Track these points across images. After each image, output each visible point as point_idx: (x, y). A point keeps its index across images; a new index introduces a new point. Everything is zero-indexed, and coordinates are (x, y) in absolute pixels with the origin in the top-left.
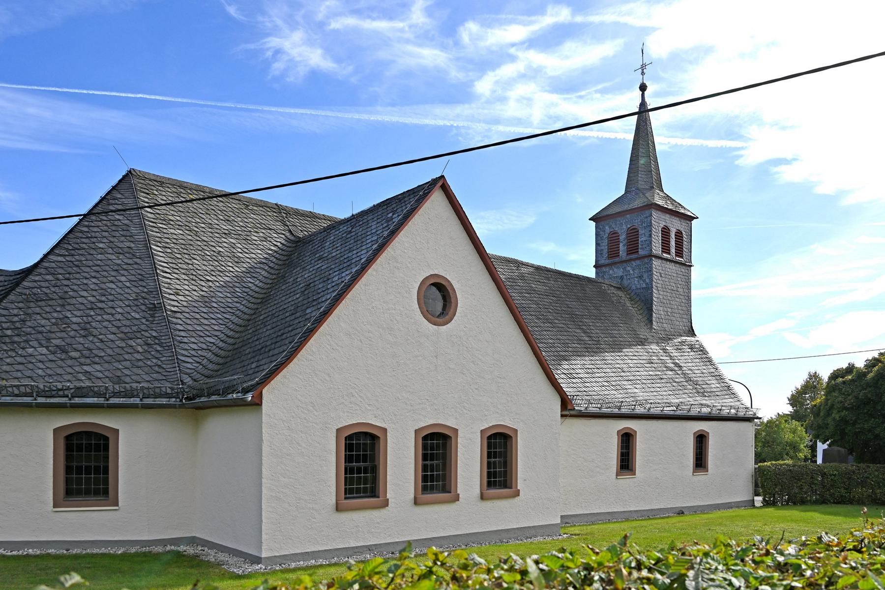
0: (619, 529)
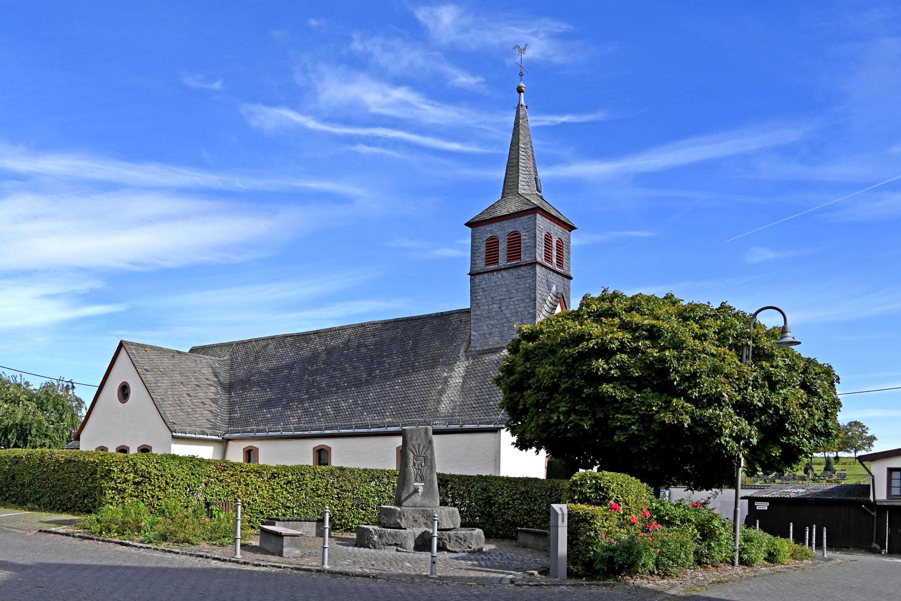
0: (264, 343)
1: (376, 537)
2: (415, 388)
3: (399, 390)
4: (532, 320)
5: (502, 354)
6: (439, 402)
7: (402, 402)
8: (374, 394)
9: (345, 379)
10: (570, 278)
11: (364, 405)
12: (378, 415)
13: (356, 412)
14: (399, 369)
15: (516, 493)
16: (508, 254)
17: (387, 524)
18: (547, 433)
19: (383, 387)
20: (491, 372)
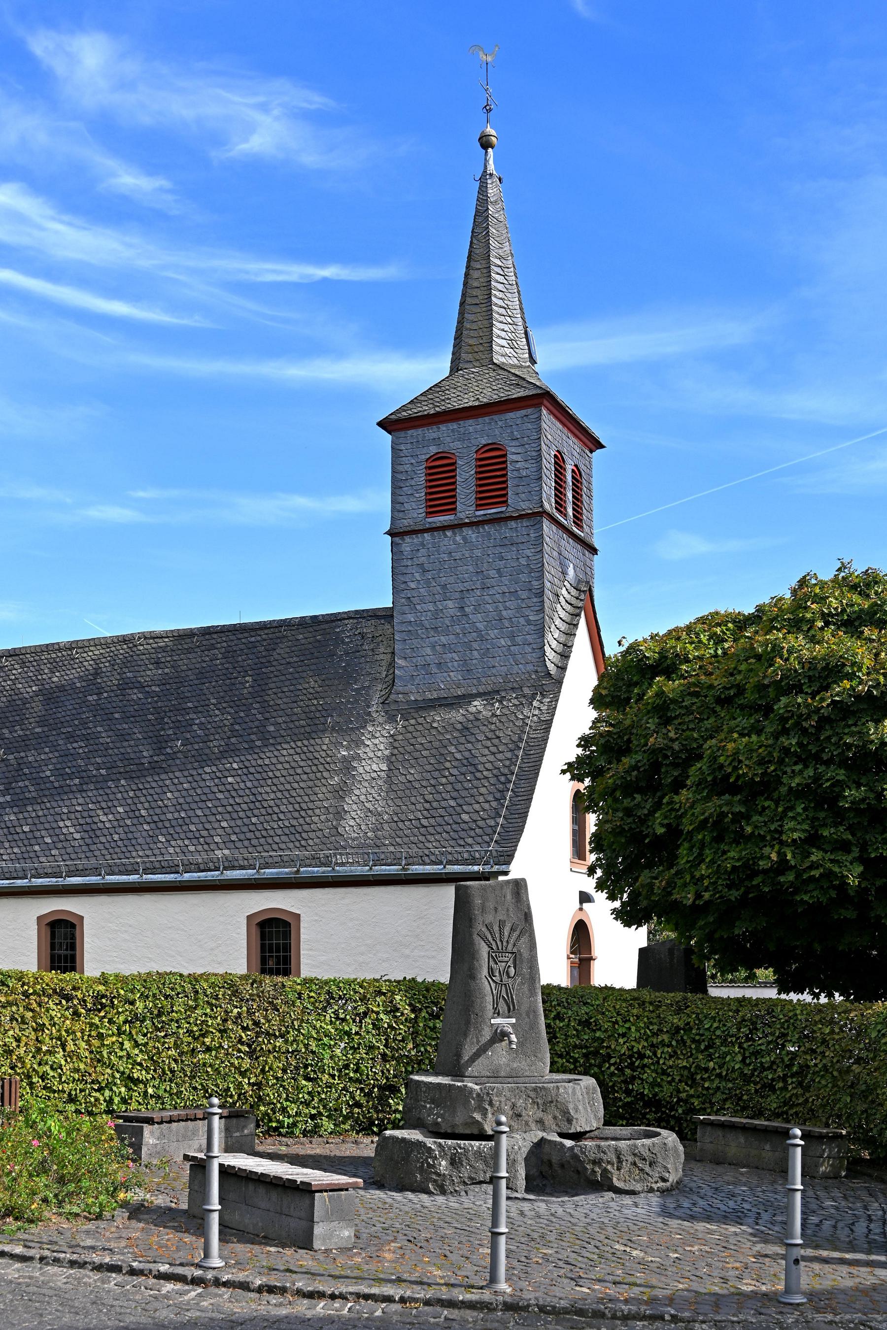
1: (443, 1163)
2: (275, 781)
3: (236, 787)
4: (535, 636)
5: (472, 709)
6: (340, 814)
7: (249, 814)
8: (177, 794)
9: (98, 760)
10: (594, 551)
11: (156, 818)
12: (195, 841)
13: (138, 835)
14: (229, 738)
15: (660, 1031)
16: (477, 492)
17: (443, 1125)
18: (743, 889)
19: (198, 778)
20: (452, 749)
